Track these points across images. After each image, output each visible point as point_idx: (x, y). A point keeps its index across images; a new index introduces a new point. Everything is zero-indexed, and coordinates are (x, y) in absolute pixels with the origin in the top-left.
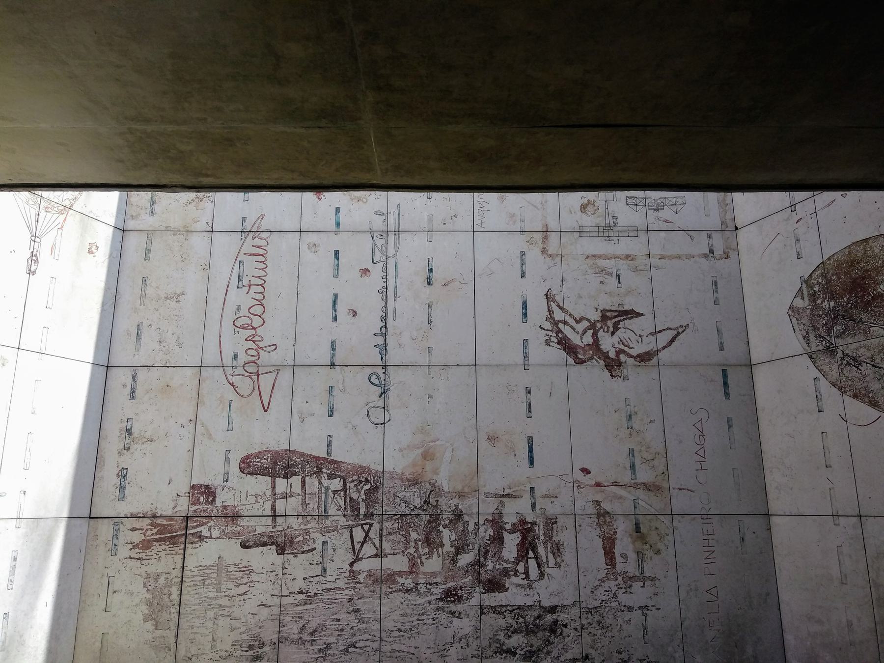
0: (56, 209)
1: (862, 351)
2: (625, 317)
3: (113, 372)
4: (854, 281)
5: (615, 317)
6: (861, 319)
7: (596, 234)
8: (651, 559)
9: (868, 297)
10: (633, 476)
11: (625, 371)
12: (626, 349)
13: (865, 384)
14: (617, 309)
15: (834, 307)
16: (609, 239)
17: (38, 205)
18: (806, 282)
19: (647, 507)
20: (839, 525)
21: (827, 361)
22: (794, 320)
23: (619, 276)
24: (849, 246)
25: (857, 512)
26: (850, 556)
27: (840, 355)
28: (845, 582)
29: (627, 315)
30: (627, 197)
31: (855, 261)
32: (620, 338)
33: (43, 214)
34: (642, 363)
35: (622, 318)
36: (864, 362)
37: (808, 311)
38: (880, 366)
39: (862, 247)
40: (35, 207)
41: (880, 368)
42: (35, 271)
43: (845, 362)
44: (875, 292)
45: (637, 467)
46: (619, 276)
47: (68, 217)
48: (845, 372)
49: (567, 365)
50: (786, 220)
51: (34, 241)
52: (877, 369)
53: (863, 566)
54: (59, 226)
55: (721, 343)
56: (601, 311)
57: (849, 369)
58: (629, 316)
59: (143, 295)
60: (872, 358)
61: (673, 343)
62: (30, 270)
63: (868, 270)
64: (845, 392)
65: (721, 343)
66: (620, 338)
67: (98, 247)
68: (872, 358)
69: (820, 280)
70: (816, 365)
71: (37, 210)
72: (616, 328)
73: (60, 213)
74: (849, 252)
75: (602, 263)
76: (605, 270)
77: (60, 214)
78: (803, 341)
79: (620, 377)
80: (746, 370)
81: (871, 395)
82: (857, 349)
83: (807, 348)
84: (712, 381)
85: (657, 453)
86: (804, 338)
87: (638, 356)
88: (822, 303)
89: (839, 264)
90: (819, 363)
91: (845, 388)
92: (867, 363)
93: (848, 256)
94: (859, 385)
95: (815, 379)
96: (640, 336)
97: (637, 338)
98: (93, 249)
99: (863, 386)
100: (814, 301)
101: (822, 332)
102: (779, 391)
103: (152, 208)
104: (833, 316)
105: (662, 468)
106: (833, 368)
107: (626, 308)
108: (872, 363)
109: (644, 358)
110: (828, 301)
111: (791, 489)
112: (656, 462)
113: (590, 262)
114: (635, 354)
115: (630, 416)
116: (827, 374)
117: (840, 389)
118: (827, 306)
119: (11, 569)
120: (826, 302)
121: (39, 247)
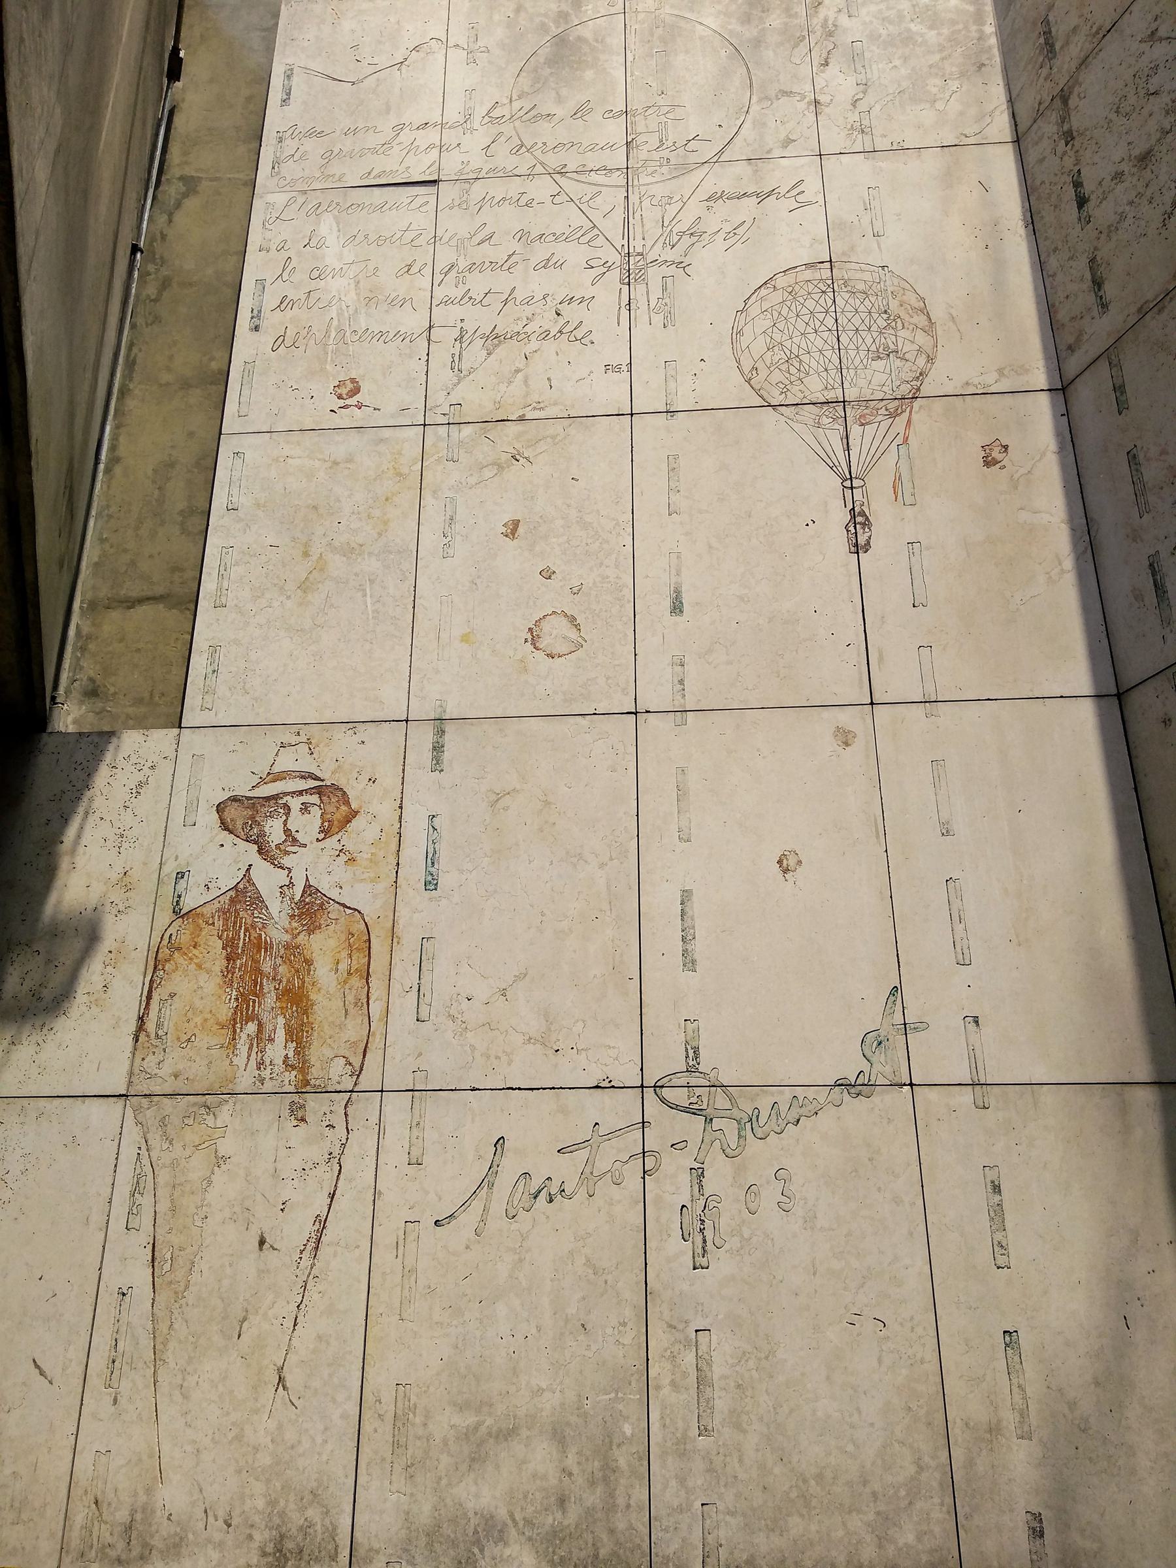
0: (883, 411)
3: (1136, 700)
17: (841, 421)
33: (855, 431)
40: (837, 426)
42: (868, 543)
47: (914, 416)
51: (852, 488)
54: (900, 440)
59: (1140, 490)
62: (856, 545)
67: (1006, 447)
71: (842, 429)
73: (893, 415)
77: (895, 417)
98: (996, 454)
103: (1101, 297)
119: (992, 1214)
121: (866, 495)
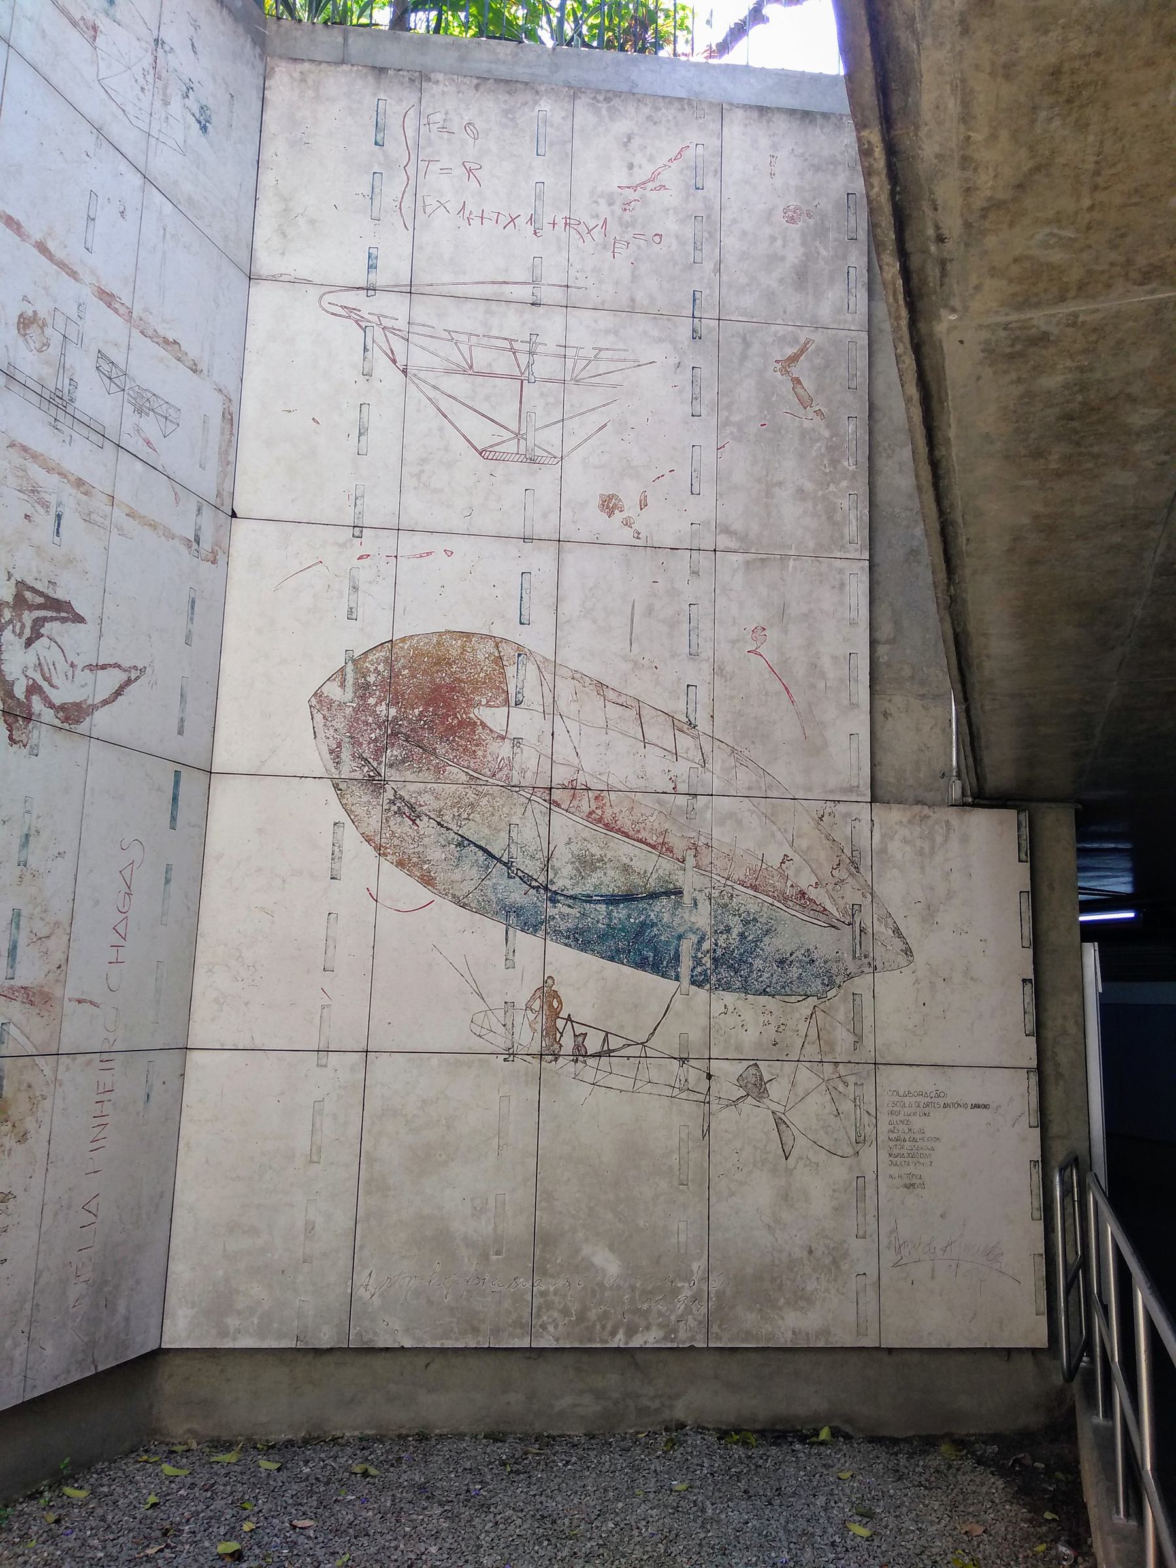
1: (426, 798)
2: (54, 614)
4: (437, 689)
5: (39, 607)
6: (435, 749)
7: (35, 399)
8: (9, 1154)
9: (453, 719)
10: (10, 971)
11: (35, 732)
12: (45, 685)
13: (420, 849)
14: (45, 590)
15: (395, 718)
16: (55, 424)
18: (355, 662)
19: (22, 1039)
20: (326, 1066)
21: (365, 799)
22: (319, 717)
23: (59, 517)
24: (440, 634)
25: (363, 1047)
26: (335, 1117)
27: (389, 794)
28: (315, 1158)
29: (58, 610)
30: (99, 351)
31: (444, 660)
32: (39, 659)
34: (66, 726)
35: (49, 614)
36: (426, 815)
37: (349, 711)
38: (450, 826)
39: (459, 641)
41: (448, 829)
43: (395, 808)
44: (464, 716)
45: (19, 951)
46: (59, 517)
48: (391, 823)
49: (551, 788)
50: (340, 545)
52: (443, 830)
53: (354, 1130)
55: (182, 718)
56: (18, 582)
57: (399, 820)
58: (63, 614)
60: (440, 813)
61: (119, 697)
63: (462, 681)
64: (385, 855)
65: (182, 718)
66: (39, 659)
68: (440, 813)
69: (381, 668)
70: (344, 801)
72: (36, 635)
74: (438, 643)
75: (37, 473)
76: (38, 492)
78: (328, 756)
79: (25, 746)
80: (204, 777)
81: (426, 867)
82: (420, 793)
83: (333, 770)
84: (159, 789)
85: (57, 924)
86: (331, 752)
87: (62, 708)
88: (376, 705)
89: (419, 654)
90: (350, 799)
91: (386, 848)
92: (430, 818)
93: (434, 648)
94: (410, 848)
95: (335, 824)
96: (72, 665)
97: (67, 667)
99: (416, 850)
100: (363, 697)
101: (367, 751)
102: (261, 831)
104: (389, 732)
105: (58, 957)
106: (373, 812)
107: (60, 594)
108: (439, 820)
109: (72, 714)
110: (388, 705)
111: (247, 1004)
112: (51, 944)
113: (16, 457)
114: (57, 702)
115: (27, 836)
116: (360, 821)
117: (378, 848)
118: (383, 713)
120: (384, 707)
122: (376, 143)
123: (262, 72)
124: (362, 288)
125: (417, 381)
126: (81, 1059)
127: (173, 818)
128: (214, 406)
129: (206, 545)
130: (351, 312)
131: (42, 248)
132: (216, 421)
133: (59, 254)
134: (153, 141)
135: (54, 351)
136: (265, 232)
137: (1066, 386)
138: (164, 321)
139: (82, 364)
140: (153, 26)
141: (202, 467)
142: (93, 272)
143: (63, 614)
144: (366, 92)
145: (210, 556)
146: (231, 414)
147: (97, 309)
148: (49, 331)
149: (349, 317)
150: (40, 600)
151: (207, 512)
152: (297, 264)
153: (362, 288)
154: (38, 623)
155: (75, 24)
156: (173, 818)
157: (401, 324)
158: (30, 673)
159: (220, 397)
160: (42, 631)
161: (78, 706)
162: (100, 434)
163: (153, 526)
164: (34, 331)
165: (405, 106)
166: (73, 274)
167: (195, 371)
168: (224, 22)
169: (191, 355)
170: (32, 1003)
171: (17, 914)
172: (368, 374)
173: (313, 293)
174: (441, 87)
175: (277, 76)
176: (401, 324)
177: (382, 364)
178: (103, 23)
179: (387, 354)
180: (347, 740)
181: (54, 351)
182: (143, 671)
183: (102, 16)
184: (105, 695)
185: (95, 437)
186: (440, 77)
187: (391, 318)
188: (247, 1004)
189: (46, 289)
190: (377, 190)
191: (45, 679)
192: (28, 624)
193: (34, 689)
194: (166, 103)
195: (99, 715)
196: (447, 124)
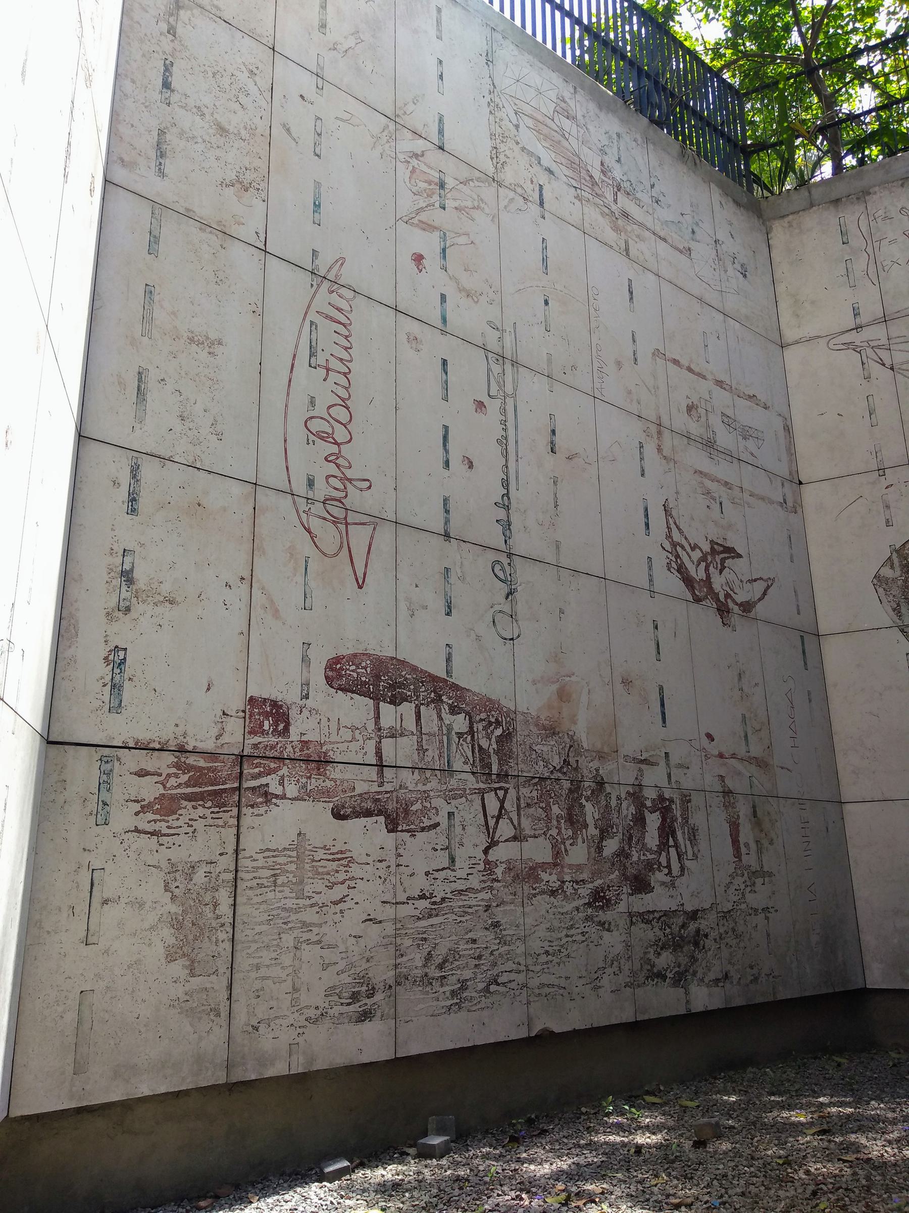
5: (722, 552)
7: (700, 446)
12: (731, 593)
18: (897, 551)
22: (881, 590)
23: (721, 503)
35: (726, 555)
37: (900, 583)
46: (721, 503)
86: (894, 610)
96: (741, 581)
107: (728, 544)
109: (747, 607)
111: (874, 773)
122: (843, 243)
123: (765, 231)
124: (853, 329)
125: (901, 372)
126: (790, 801)
127: (805, 664)
128: (778, 423)
129: (790, 504)
130: (848, 345)
131: (689, 369)
132: (781, 433)
133: (697, 370)
134: (723, 293)
135: (703, 419)
136: (786, 317)
137: (597, 1133)
138: (747, 386)
139: (715, 421)
140: (711, 233)
141: (780, 460)
142: (712, 373)
143: (732, 555)
144: (831, 217)
145: (793, 509)
146: (788, 426)
147: (717, 390)
148: (699, 410)
149: (849, 348)
150: (722, 549)
151: (787, 484)
152: (809, 330)
153: (853, 329)
154: (723, 561)
155: (681, 252)
156: (805, 664)
157: (884, 341)
158: (724, 588)
159: (781, 418)
160: (725, 565)
161: (747, 602)
162: (729, 455)
163: (763, 499)
164: (693, 412)
165: (857, 215)
166: (704, 377)
167: (766, 408)
168: (742, 215)
169: (763, 400)
170: (760, 766)
171: (744, 716)
172: (868, 378)
173: (823, 342)
174: (878, 194)
175: (774, 230)
176: (884, 341)
177: (875, 369)
178: (693, 245)
179: (878, 362)
180: (903, 601)
181: (703, 419)
182: (773, 580)
183: (691, 241)
184: (758, 595)
185: (728, 458)
186: (877, 189)
187: (876, 340)
188: (874, 773)
189: (694, 389)
190: (850, 270)
191: (731, 590)
192: (719, 562)
193: (727, 596)
194: (726, 271)
195: (759, 606)
196: (888, 214)
